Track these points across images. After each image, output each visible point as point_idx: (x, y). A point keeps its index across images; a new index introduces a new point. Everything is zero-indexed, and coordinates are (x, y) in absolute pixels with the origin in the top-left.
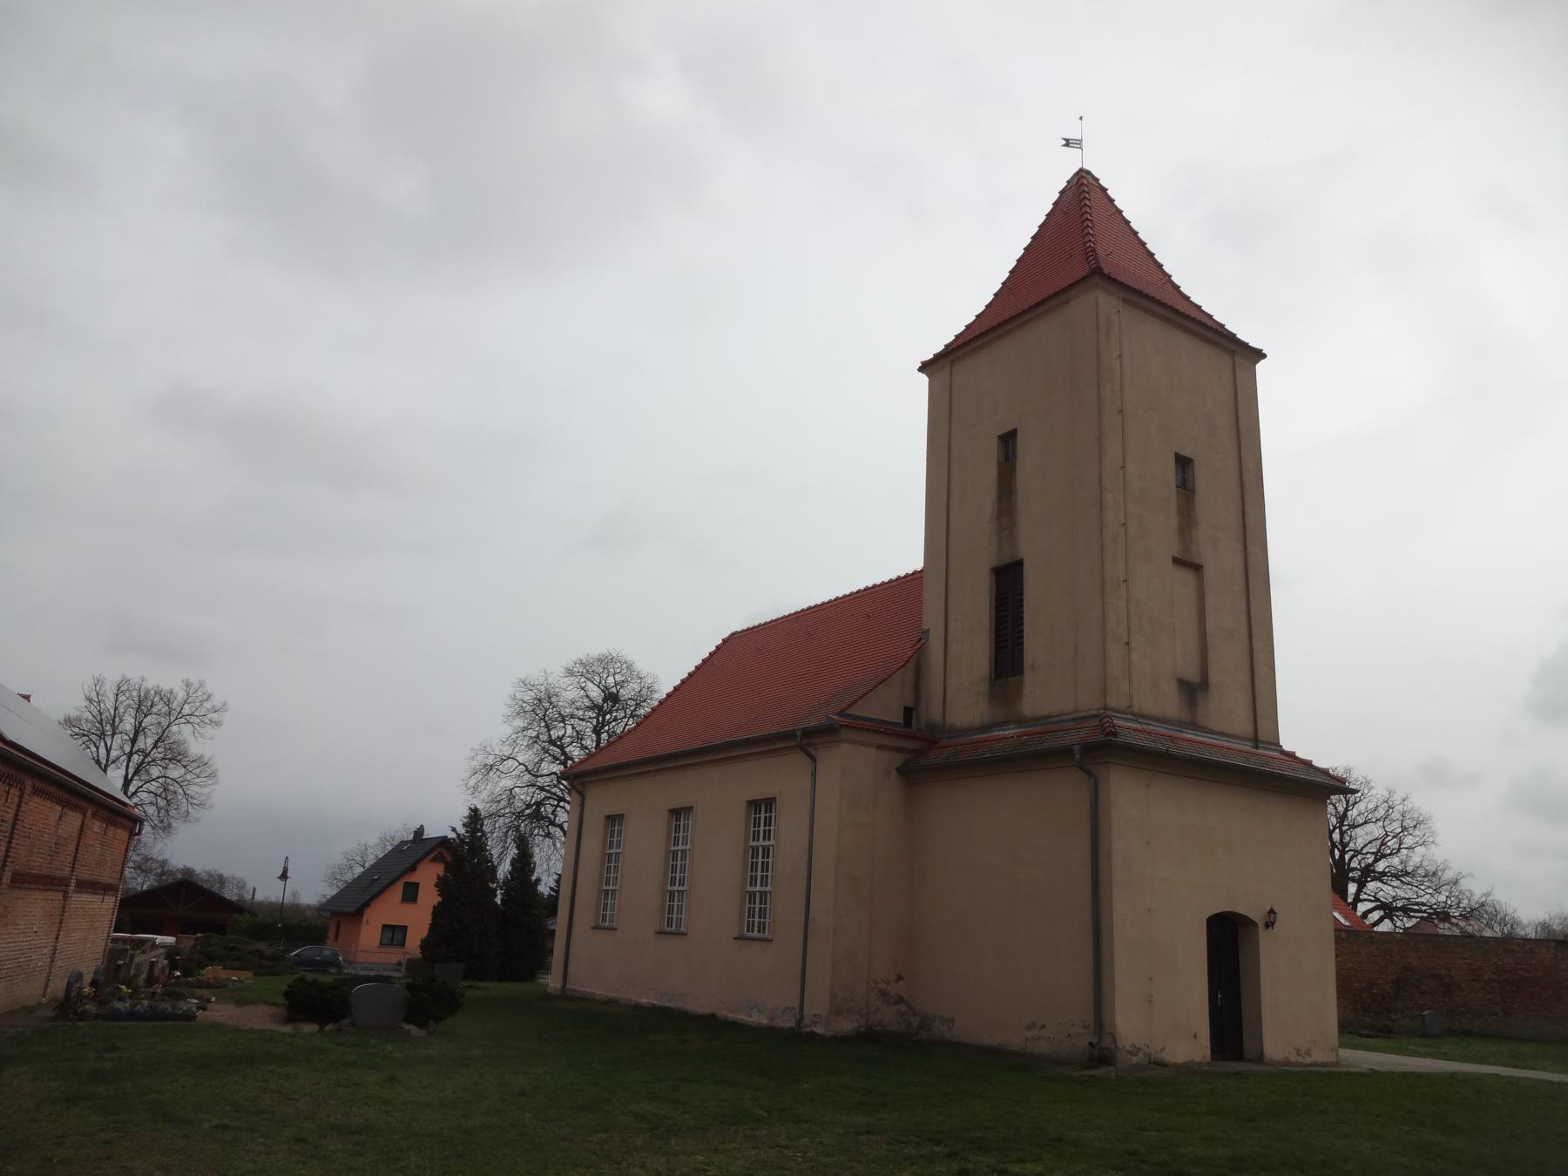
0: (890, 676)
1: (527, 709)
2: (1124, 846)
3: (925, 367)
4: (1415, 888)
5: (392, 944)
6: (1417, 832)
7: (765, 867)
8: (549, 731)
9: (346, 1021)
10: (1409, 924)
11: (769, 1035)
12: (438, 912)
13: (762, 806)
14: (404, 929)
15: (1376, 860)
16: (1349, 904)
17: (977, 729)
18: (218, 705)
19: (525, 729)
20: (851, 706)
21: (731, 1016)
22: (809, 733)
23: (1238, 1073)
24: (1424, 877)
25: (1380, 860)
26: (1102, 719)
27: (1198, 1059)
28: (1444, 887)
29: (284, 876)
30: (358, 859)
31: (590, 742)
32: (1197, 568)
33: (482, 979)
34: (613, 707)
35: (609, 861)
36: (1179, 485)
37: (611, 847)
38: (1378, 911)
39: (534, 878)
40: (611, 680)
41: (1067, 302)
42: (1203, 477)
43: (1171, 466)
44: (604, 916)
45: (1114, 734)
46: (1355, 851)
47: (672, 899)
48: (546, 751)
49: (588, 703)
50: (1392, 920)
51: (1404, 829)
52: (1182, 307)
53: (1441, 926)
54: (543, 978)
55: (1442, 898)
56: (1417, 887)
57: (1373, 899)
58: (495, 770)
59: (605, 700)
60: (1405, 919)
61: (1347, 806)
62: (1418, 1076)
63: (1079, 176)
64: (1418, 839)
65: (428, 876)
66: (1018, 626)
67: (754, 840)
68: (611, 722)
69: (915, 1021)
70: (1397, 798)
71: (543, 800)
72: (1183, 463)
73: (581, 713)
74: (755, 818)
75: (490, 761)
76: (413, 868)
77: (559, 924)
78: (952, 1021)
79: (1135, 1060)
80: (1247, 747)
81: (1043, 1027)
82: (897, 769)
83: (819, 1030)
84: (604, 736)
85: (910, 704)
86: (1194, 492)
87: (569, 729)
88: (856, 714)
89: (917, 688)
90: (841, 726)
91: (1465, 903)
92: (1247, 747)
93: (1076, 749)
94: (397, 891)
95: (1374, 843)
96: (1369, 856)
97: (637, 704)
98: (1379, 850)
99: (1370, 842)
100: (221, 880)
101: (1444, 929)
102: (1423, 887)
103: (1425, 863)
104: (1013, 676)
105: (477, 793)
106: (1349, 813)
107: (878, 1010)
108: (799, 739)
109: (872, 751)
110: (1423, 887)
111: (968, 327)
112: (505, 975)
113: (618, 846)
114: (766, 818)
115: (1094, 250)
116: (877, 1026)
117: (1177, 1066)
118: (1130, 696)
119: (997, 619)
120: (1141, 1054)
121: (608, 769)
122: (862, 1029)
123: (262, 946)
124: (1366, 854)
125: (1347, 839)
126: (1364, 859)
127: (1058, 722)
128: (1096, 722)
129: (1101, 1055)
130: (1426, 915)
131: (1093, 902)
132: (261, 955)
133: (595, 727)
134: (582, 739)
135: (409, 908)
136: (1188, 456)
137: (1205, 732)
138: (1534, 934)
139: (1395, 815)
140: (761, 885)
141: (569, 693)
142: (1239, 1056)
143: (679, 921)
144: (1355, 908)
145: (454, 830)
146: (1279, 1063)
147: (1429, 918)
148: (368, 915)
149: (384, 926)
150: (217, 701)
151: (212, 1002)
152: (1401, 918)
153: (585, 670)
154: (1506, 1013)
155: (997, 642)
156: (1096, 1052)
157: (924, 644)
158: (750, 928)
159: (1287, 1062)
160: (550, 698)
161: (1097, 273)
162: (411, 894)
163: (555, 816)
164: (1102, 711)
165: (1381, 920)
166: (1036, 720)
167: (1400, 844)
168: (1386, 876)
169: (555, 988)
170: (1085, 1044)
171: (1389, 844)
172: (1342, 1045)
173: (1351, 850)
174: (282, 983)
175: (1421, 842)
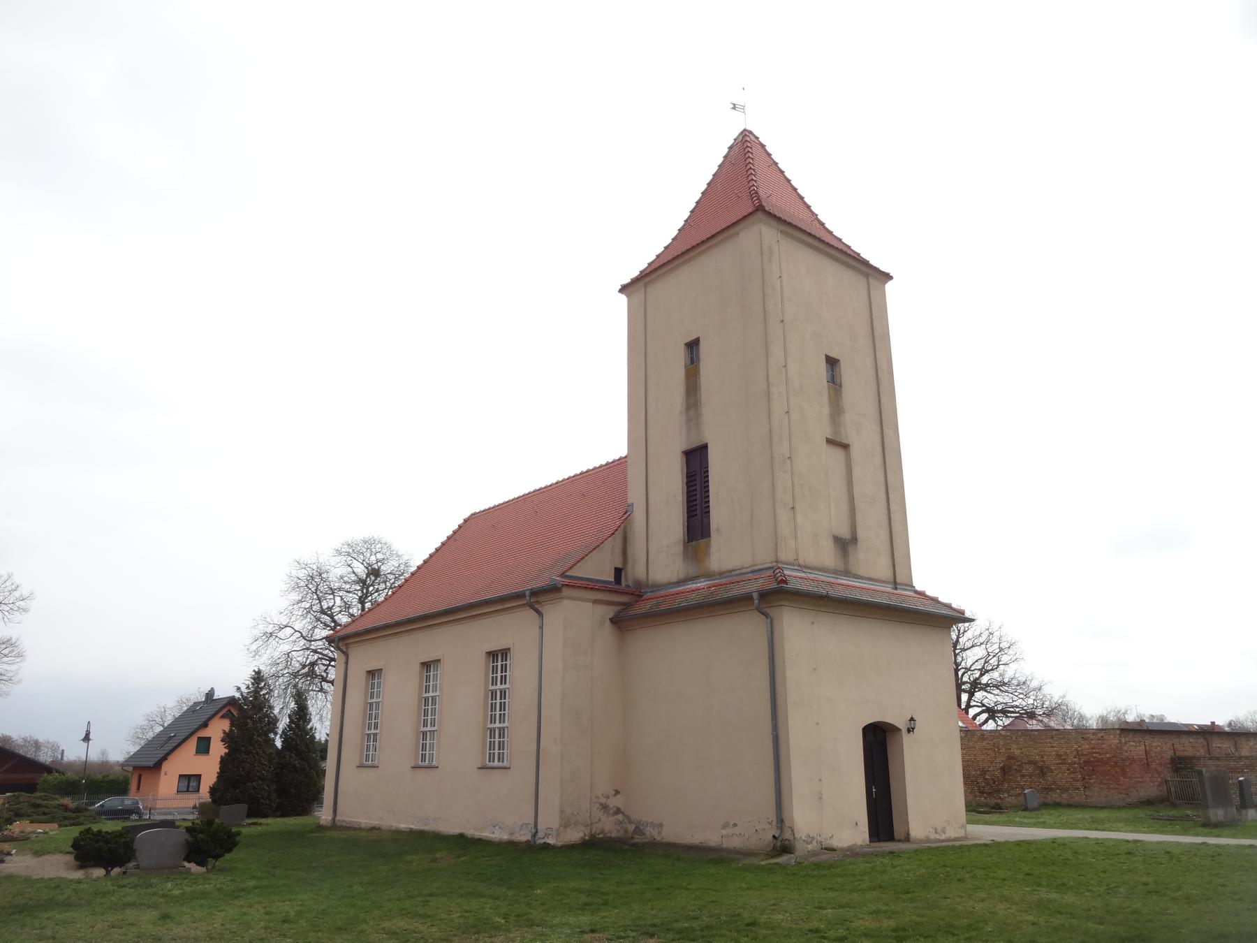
0: (602, 543)
1: (301, 585)
2: (795, 675)
3: (624, 289)
4: (1010, 695)
5: (188, 791)
6: (1011, 652)
7: (503, 707)
8: (320, 602)
9: (131, 865)
10: (1007, 722)
11: (510, 847)
12: (224, 761)
13: (498, 656)
14: (198, 777)
15: (982, 675)
16: (963, 710)
17: (674, 583)
18: (26, 594)
19: (301, 601)
20: (571, 568)
21: (477, 834)
22: (535, 593)
23: (891, 853)
24: (1017, 686)
25: (984, 674)
26: (775, 570)
27: (859, 842)
28: (1032, 693)
29: (87, 738)
30: (158, 720)
31: (355, 611)
32: (845, 447)
33: (265, 816)
34: (376, 580)
35: (371, 710)
36: (830, 380)
37: (372, 697)
38: (984, 714)
39: (309, 727)
40: (373, 559)
41: (737, 234)
42: (847, 373)
43: (823, 365)
44: (423, 757)
45: (785, 582)
46: (966, 668)
47: (424, 738)
48: (318, 620)
49: (353, 578)
50: (995, 721)
51: (1001, 650)
52: (827, 238)
53: (1030, 722)
54: (318, 811)
55: (1031, 701)
56: (1012, 694)
57: (980, 705)
58: (274, 637)
59: (368, 575)
60: (1004, 719)
61: (959, 635)
62: (1029, 843)
63: (744, 134)
64: (1011, 657)
65: (218, 729)
66: (705, 497)
67: (492, 685)
68: (374, 593)
69: (631, 828)
70: (994, 628)
71: (317, 661)
72: (832, 362)
73: (348, 586)
74: (493, 666)
75: (269, 630)
76: (205, 725)
77: (329, 765)
78: (661, 825)
79: (810, 847)
80: (889, 589)
81: (735, 825)
82: (610, 619)
83: (551, 841)
84: (368, 605)
85: (619, 566)
86: (841, 386)
87: (338, 600)
88: (575, 575)
89: (624, 552)
90: (563, 585)
91: (1047, 704)
92: (889, 589)
93: (755, 595)
94: (192, 744)
95: (979, 662)
96: (976, 672)
97: (396, 578)
98: (983, 667)
99: (977, 661)
100: (37, 745)
101: (1033, 725)
102: (1016, 694)
103: (1017, 676)
104: (702, 539)
105: (257, 657)
106: (960, 640)
107: (600, 820)
108: (528, 598)
109: (589, 605)
110: (1016, 694)
111: (658, 256)
112: (284, 811)
113: (378, 696)
114: (502, 665)
115: (756, 193)
116: (599, 834)
117: (842, 849)
118: (797, 550)
119: (688, 492)
120: (814, 842)
121: (368, 631)
122: (587, 838)
123: (67, 801)
124: (973, 670)
125: (959, 659)
126: (972, 674)
127: (737, 575)
128: (770, 573)
129: (783, 847)
130: (1018, 715)
131: (772, 720)
132: (66, 808)
133: (360, 597)
134: (349, 608)
135: (203, 759)
136: (835, 357)
137: (856, 578)
138: (1095, 725)
139: (995, 639)
140: (500, 722)
141: (338, 571)
142: (890, 837)
143: (431, 756)
144: (967, 713)
145: (239, 689)
146: (921, 841)
147: (1020, 718)
148: (166, 767)
149: (180, 776)
150: (24, 591)
151: (12, 855)
152: (1001, 718)
153: (351, 551)
154: (1085, 787)
155: (688, 512)
156: (779, 844)
157: (629, 515)
158: (491, 758)
159: (928, 840)
160: (320, 575)
161: (760, 209)
162: (204, 746)
163: (327, 673)
164: (775, 564)
165: (986, 721)
166: (721, 574)
167: (999, 661)
168: (989, 686)
169: (326, 820)
170: (770, 838)
171: (990, 662)
172: (970, 822)
173: (962, 668)
174: (75, 832)
175: (1014, 659)
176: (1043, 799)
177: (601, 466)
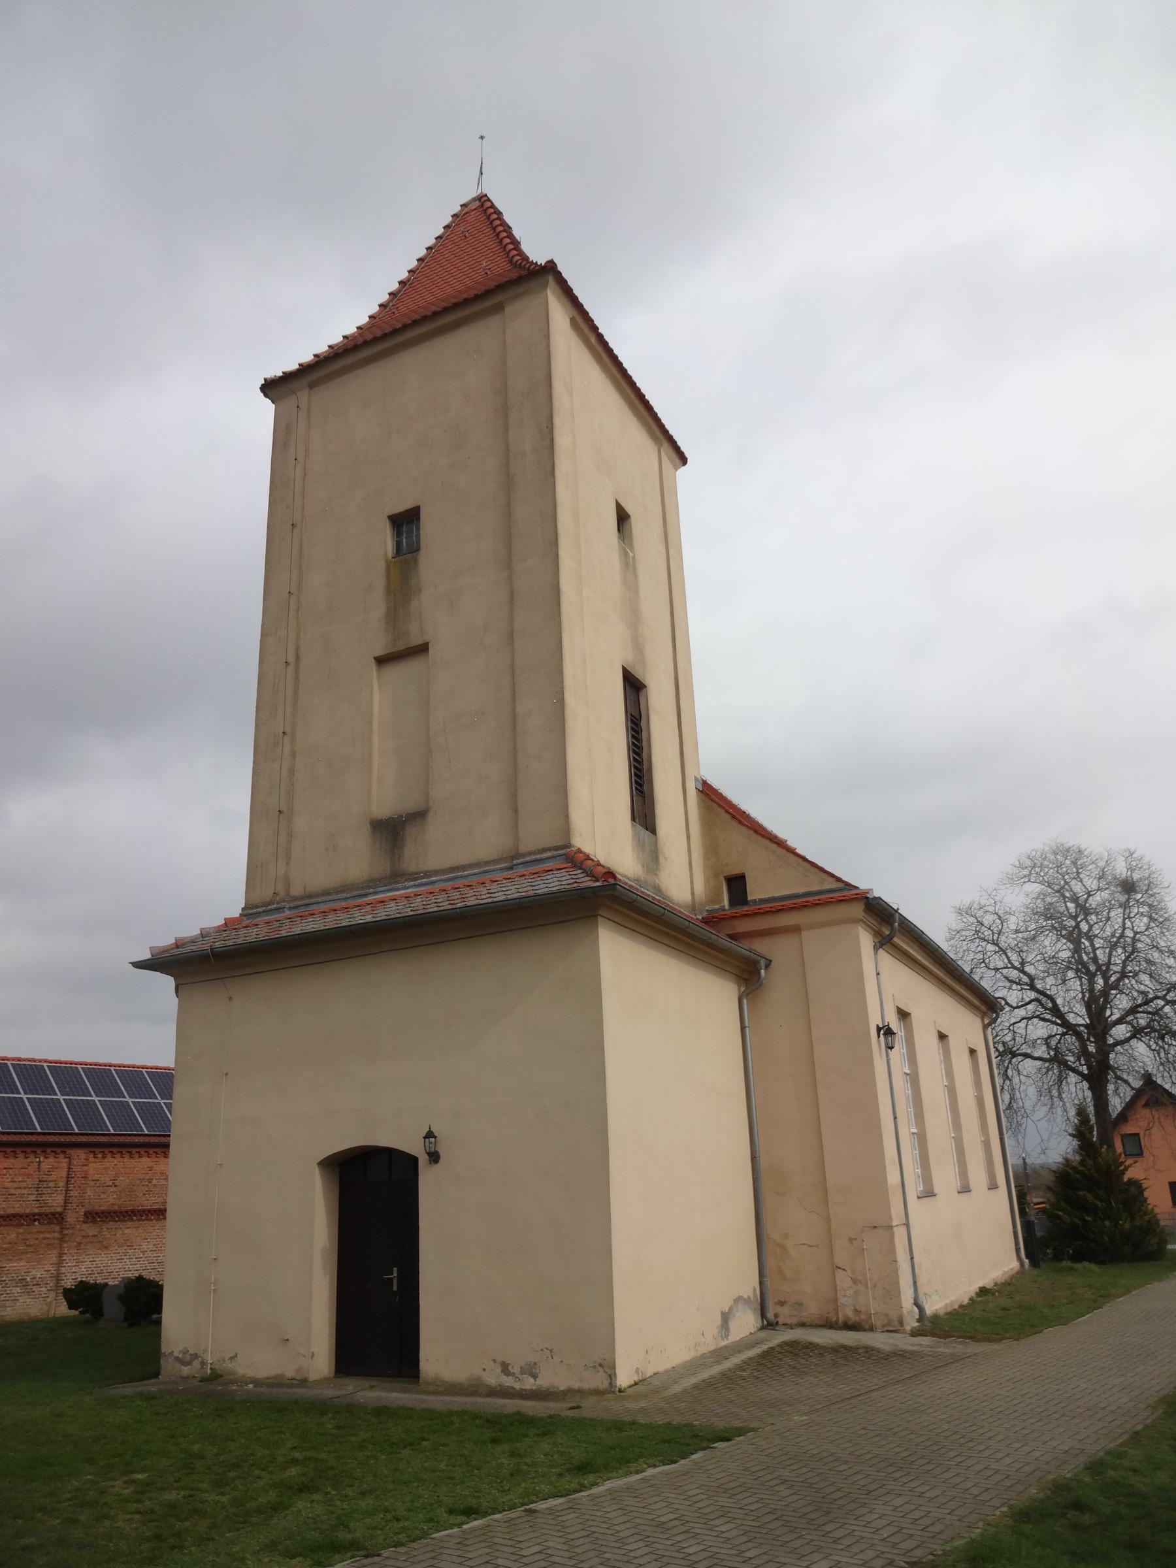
3: (270, 388)
79: (186, 1370)
120: (196, 1363)
146: (453, 1389)
176: (981, 1312)
177: (516, 244)
